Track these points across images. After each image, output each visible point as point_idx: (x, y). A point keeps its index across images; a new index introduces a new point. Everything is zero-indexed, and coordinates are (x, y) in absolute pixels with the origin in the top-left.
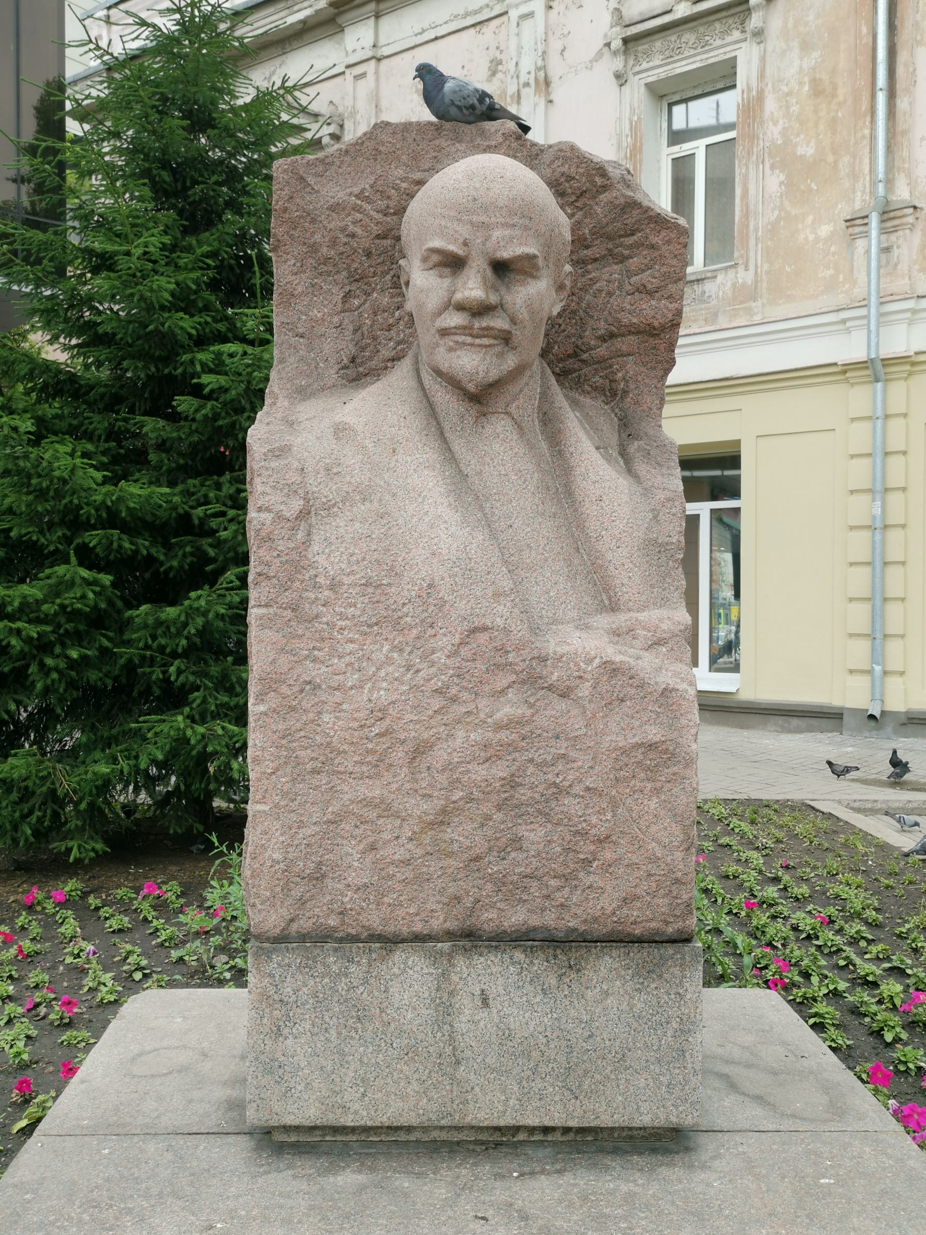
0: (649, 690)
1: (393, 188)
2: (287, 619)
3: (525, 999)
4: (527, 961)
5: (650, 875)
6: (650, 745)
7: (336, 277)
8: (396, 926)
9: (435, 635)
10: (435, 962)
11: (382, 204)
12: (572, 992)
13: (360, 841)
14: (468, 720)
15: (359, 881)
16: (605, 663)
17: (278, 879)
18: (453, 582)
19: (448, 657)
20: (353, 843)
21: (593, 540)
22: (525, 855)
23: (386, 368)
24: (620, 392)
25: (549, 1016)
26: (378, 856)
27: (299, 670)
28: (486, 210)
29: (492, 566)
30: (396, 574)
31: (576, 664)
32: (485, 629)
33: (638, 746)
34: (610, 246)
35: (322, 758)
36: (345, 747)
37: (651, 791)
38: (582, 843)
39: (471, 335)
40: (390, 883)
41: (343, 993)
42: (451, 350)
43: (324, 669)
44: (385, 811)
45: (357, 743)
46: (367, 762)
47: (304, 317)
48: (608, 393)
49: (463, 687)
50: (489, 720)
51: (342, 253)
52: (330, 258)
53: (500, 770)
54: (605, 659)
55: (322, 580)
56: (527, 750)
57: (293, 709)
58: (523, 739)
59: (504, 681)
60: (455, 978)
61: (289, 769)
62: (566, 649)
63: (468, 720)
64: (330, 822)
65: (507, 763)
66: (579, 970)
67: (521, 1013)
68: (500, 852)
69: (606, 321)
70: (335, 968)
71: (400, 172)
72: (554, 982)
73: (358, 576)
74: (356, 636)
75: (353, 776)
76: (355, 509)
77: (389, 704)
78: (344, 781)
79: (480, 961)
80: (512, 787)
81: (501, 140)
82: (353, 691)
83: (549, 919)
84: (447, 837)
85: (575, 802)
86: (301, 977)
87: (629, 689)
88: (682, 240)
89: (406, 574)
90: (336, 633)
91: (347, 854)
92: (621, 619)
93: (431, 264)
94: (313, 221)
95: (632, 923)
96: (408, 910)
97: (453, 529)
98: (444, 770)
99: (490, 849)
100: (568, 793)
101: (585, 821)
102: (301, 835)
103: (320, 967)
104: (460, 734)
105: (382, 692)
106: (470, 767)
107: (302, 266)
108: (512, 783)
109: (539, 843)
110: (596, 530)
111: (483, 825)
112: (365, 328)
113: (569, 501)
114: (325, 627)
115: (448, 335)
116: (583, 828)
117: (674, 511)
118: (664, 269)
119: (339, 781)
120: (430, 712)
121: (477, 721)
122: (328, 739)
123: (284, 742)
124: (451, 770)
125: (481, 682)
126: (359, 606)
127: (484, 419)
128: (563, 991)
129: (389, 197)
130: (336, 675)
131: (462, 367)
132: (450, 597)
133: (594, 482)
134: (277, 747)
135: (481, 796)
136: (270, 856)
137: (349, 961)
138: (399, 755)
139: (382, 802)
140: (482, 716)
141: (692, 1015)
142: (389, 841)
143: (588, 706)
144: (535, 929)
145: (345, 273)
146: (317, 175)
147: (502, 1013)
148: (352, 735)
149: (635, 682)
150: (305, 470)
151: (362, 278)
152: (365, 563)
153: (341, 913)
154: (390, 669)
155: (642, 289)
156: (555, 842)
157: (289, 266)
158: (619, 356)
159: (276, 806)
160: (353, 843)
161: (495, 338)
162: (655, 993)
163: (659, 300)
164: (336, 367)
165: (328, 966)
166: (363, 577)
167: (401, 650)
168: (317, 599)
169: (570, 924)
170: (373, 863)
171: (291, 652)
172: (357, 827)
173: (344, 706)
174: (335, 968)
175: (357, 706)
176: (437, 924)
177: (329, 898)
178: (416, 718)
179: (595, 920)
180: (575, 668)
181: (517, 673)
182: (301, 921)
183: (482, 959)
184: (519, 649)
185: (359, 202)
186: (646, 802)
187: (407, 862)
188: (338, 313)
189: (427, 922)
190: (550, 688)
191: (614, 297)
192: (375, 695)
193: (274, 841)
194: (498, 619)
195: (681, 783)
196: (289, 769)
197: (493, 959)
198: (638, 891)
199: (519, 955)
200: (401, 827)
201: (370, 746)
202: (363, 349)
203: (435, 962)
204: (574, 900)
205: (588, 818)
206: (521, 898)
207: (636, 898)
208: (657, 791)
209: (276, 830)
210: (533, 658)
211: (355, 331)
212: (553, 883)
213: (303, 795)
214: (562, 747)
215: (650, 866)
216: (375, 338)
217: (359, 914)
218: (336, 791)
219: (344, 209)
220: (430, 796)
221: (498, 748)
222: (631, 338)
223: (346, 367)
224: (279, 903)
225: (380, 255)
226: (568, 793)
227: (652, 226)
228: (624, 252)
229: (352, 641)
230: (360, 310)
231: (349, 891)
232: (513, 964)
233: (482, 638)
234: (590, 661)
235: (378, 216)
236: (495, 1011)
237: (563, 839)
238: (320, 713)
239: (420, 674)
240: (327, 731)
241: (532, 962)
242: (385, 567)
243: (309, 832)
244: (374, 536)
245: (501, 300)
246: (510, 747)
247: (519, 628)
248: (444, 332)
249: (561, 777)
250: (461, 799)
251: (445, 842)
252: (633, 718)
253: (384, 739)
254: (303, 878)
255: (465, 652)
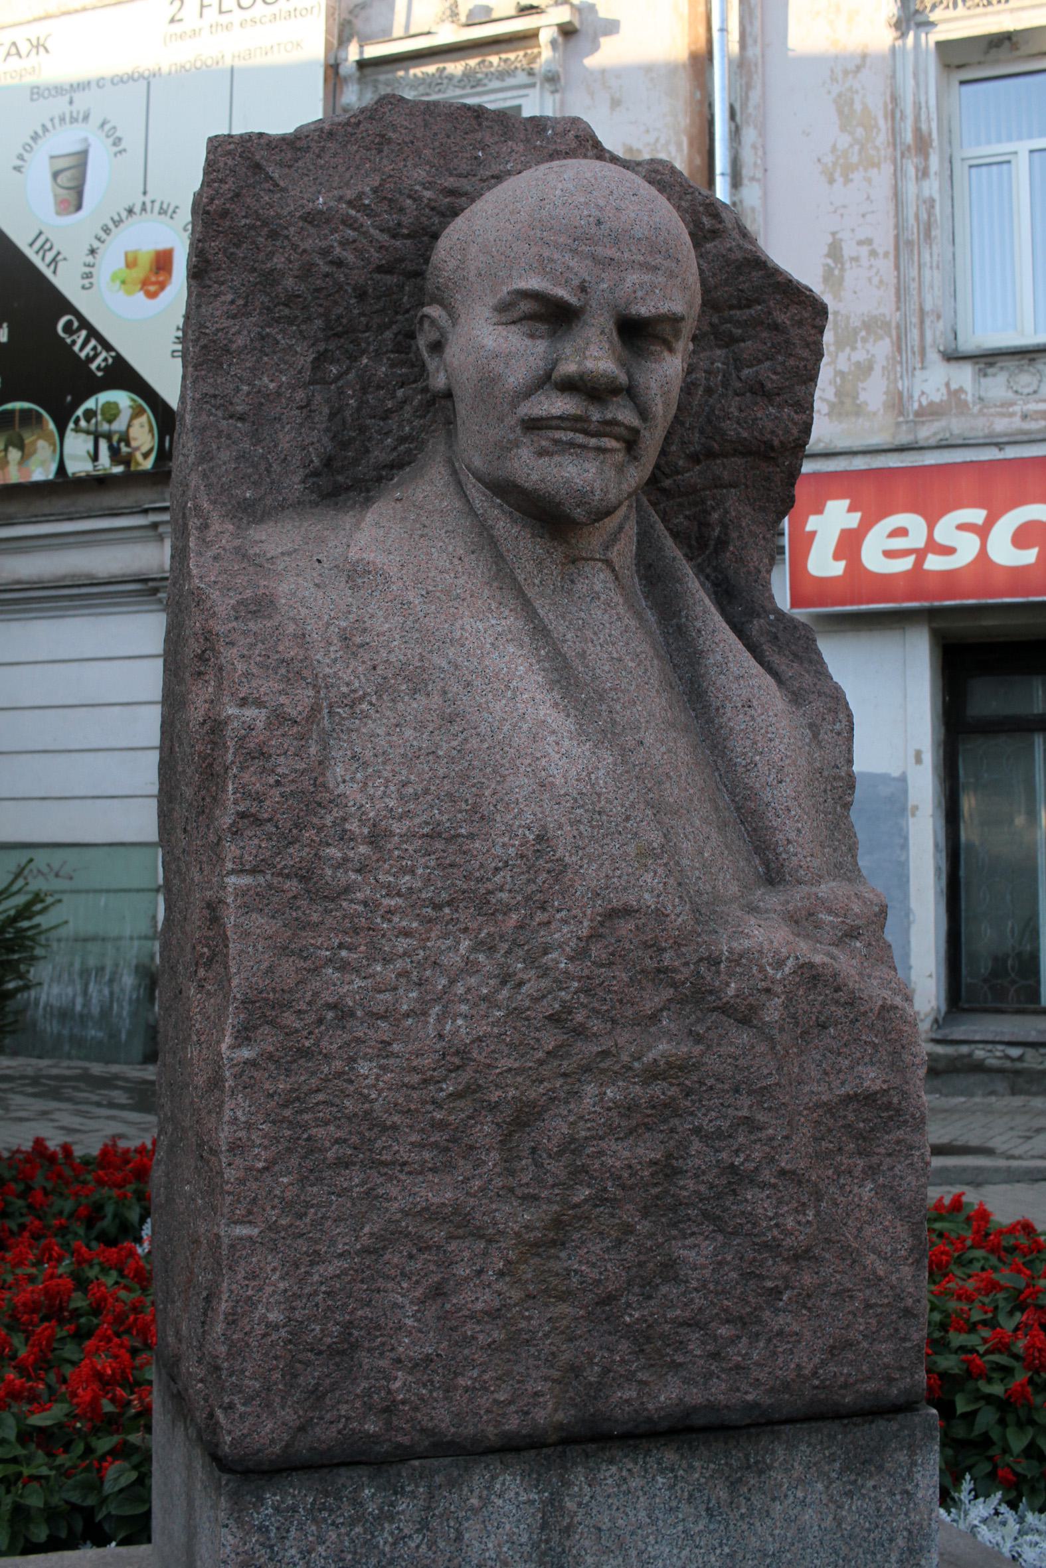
0: (862, 1009)
1: (410, 197)
2: (290, 895)
3: (680, 1528)
4: (684, 1464)
5: (869, 1306)
6: (866, 1098)
7: (303, 327)
8: (475, 1425)
9: (549, 923)
10: (538, 1480)
11: (390, 219)
12: (751, 1509)
13: (417, 1282)
14: (602, 1065)
15: (416, 1353)
16: (802, 966)
17: (276, 1358)
18: (576, 833)
19: (571, 959)
20: (405, 1285)
21: (740, 769)
22: (682, 1288)
23: (379, 479)
24: (712, 543)
25: (718, 1552)
26: (448, 1306)
27: (316, 984)
28: (616, 241)
29: (632, 806)
30: (482, 818)
31: (762, 969)
32: (627, 912)
33: (848, 1099)
34: (715, 320)
35: (355, 1139)
36: (396, 1118)
37: (863, 1171)
38: (770, 1262)
39: (586, 433)
40: (466, 1352)
41: (387, 1549)
42: (542, 453)
43: (358, 982)
44: (458, 1227)
45: (417, 1110)
46: (431, 1145)
47: (245, 388)
48: (694, 543)
49: (596, 1011)
50: (636, 1065)
51: (318, 290)
52: (299, 296)
53: (648, 1150)
54: (801, 961)
55: (353, 826)
56: (692, 1114)
57: (305, 1053)
58: (687, 1095)
59: (656, 999)
60: (570, 1505)
61: (294, 1161)
62: (747, 943)
63: (602, 1065)
64: (366, 1251)
65: (661, 1136)
66: (761, 1472)
67: (675, 1551)
68: (643, 1287)
69: (702, 432)
70: (372, 1507)
71: (421, 174)
72: (724, 1495)
73: (417, 821)
74: (415, 925)
75: (407, 1169)
76: (400, 706)
77: (473, 1042)
78: (391, 1178)
79: (609, 1473)
80: (666, 1175)
81: (574, 145)
82: (410, 1021)
83: (718, 1391)
84: (556, 1266)
85: (763, 1195)
86: (314, 1528)
87: (833, 1008)
88: (818, 322)
89: (498, 818)
90: (379, 920)
91: (395, 1305)
92: (798, 896)
93: (515, 314)
94: (273, 235)
95: (841, 1387)
96: (496, 1396)
97: (567, 743)
98: (560, 1153)
99: (630, 1283)
100: (751, 1181)
101: (777, 1225)
102: (316, 1278)
103: (348, 1511)
104: (590, 1089)
105: (460, 1022)
106: (603, 1144)
107: (245, 305)
108: (668, 1170)
109: (704, 1267)
110: (745, 754)
111: (619, 1243)
112: (348, 413)
113: (699, 706)
114: (360, 908)
115: (539, 429)
116: (774, 1238)
117: (838, 727)
118: (791, 362)
119: (382, 1179)
120: (540, 1055)
121: (616, 1068)
122: (367, 1106)
123: (287, 1113)
124: (573, 1152)
125: (620, 1001)
126: (420, 871)
127: (572, 569)
128: (738, 1508)
129: (401, 210)
130: (380, 992)
131: (567, 481)
132: (574, 859)
133: (738, 678)
134: (274, 1122)
135: (619, 1193)
136: (263, 1317)
137: (396, 1493)
138: (485, 1130)
139: (456, 1212)
140: (625, 1058)
141: (925, 1523)
142: (467, 1279)
143: (778, 1037)
144: (695, 1409)
145: (319, 323)
146: (281, 164)
147: (645, 1556)
148: (408, 1098)
149: (842, 996)
150: (308, 639)
151: (347, 332)
152: (429, 798)
153: (387, 1410)
154: (473, 981)
155: (759, 390)
156: (728, 1263)
157: (224, 303)
158: (716, 487)
159: (273, 1227)
160: (405, 1285)
161: (617, 438)
162: (873, 1495)
163: (780, 407)
164: (301, 473)
165: (361, 1504)
166: (427, 823)
167: (492, 949)
168: (346, 859)
169: (749, 1397)
170: (439, 1318)
171: (301, 954)
172: (411, 1257)
173: (396, 1047)
174: (372, 1507)
175: (417, 1045)
176: (543, 1415)
177: (365, 1384)
178: (516, 1065)
179: (786, 1386)
180: (760, 976)
181: (674, 985)
182: (317, 1429)
183: (614, 1469)
184: (680, 945)
185: (353, 212)
186: (856, 1190)
187: (493, 1315)
188: (305, 386)
189: (527, 1413)
190: (725, 1010)
191: (716, 396)
192: (448, 1027)
193: (269, 1289)
194: (647, 896)
195: (907, 1157)
196: (294, 1161)
197: (631, 1466)
198: (852, 1335)
199: (670, 1456)
200: (485, 1254)
201: (438, 1116)
202: (344, 445)
203: (538, 1480)
204: (755, 1357)
205: (781, 1220)
206: (673, 1361)
207: (849, 1344)
208: (872, 1171)
209: (274, 1270)
210: (701, 960)
211: (332, 416)
212: (723, 1331)
213: (319, 1205)
214: (744, 1105)
215: (868, 1292)
216: (362, 429)
217: (416, 1409)
218: (377, 1197)
219: (328, 221)
220: (535, 1198)
221: (649, 1112)
222: (739, 461)
223: (316, 474)
224: (278, 1400)
225: (378, 298)
226: (751, 1181)
227: (778, 297)
228: (734, 330)
229: (407, 933)
230: (340, 383)
231: (399, 1369)
232: (662, 1471)
233: (626, 927)
234: (779, 964)
235: (384, 238)
236: (634, 1553)
237: (741, 1259)
238: (352, 1060)
239: (524, 990)
240: (366, 1091)
241: (691, 1466)
242: (464, 806)
243: (331, 1270)
244: (441, 753)
245: (553, 1504)
246: (669, 1109)
247: (678, 910)
248: (533, 425)
249: (742, 1157)
250: (586, 1201)
251: (557, 1275)
252: (839, 1054)
253: (460, 1104)
254: (320, 1353)
255: (596, 950)
